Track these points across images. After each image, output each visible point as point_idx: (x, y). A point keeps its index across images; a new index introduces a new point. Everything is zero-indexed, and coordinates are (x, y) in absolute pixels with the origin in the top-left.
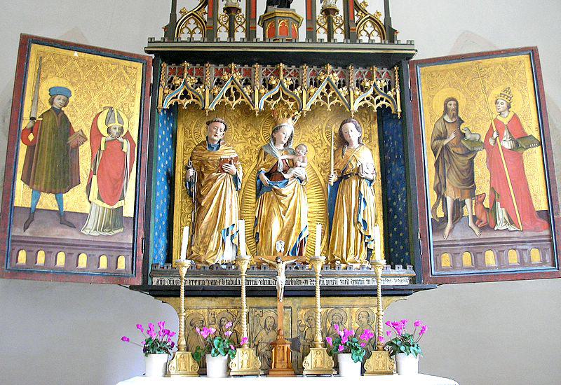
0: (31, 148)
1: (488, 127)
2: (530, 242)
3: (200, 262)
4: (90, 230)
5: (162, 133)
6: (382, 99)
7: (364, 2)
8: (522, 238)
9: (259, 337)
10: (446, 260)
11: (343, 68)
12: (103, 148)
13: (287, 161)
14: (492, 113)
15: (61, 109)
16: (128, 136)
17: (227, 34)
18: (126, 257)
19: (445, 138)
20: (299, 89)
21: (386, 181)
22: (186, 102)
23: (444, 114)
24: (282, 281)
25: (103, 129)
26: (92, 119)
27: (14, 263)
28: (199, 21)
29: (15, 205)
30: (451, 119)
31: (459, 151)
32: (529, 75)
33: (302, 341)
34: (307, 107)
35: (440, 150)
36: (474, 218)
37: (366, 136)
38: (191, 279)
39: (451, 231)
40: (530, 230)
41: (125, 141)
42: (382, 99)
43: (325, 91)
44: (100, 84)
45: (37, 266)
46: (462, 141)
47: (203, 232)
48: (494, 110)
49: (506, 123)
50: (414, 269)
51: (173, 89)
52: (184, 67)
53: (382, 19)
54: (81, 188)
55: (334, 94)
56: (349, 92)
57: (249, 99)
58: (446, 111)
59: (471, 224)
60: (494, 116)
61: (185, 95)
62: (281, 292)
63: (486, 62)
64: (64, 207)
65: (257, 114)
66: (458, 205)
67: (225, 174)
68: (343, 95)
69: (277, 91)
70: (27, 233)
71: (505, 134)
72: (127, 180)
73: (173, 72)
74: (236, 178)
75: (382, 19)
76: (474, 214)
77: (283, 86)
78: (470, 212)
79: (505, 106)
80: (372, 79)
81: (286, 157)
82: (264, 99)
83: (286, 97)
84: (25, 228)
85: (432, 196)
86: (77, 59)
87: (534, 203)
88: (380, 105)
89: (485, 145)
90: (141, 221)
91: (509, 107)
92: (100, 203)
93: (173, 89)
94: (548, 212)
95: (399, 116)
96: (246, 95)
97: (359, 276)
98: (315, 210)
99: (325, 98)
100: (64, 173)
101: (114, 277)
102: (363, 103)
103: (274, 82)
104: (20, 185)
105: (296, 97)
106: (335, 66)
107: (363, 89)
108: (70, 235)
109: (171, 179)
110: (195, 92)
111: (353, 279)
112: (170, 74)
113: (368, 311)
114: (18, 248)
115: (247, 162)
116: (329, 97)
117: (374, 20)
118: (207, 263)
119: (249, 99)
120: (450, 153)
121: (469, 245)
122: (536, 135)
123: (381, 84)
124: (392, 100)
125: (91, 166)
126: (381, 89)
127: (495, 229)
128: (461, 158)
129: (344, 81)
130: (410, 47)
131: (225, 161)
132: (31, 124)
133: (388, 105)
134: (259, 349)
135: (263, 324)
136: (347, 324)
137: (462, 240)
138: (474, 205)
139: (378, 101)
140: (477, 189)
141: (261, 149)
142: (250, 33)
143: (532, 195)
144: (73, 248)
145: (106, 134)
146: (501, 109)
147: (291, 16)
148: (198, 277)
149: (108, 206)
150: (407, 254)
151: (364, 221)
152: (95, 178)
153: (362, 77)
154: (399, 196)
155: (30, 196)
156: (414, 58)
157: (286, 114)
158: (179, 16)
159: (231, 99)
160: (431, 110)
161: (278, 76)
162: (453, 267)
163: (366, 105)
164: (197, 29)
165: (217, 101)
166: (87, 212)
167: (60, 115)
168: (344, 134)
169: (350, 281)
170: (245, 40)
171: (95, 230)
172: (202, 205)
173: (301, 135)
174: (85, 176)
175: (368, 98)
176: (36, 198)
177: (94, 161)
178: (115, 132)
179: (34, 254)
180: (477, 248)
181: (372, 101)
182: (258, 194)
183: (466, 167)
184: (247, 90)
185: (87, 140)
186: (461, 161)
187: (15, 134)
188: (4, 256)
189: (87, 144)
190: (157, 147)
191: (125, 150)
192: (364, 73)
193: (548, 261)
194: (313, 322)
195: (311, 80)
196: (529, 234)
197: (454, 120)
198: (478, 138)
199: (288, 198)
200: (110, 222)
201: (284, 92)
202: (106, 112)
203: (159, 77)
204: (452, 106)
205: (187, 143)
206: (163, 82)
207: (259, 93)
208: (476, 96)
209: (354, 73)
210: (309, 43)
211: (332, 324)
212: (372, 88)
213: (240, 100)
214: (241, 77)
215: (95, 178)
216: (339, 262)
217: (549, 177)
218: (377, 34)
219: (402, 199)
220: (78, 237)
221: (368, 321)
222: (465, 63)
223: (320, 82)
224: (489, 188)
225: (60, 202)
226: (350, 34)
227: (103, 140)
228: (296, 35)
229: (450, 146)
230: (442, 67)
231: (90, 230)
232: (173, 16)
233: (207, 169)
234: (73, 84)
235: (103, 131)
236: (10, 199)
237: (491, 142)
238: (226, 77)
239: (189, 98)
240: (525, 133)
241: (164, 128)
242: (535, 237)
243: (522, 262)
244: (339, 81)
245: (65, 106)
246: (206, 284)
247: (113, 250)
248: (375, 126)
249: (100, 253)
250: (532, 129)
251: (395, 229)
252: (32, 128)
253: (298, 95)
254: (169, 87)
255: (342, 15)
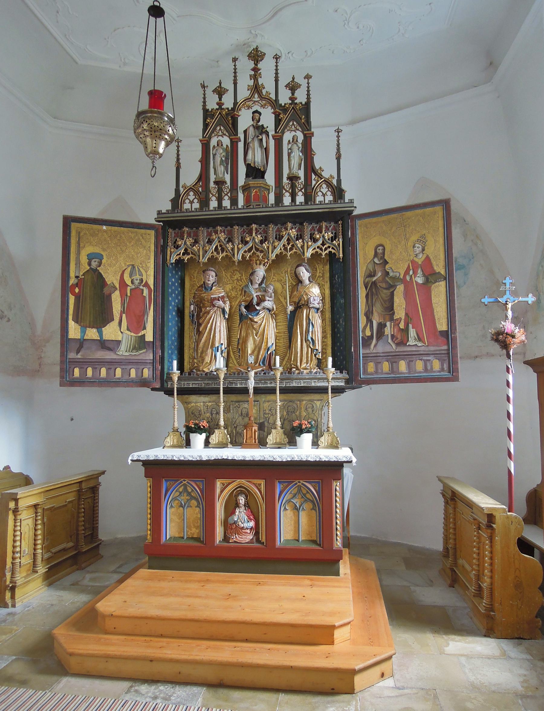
0: (78, 298)
1: (406, 266)
2: (433, 354)
3: (199, 371)
4: (123, 351)
5: (172, 280)
6: (329, 247)
7: (320, 168)
8: (428, 351)
9: (238, 421)
10: (371, 367)
11: (300, 225)
12: (129, 294)
13: (260, 296)
14: (410, 256)
15: (97, 268)
16: (147, 285)
17: (290, 198)
18: (149, 369)
19: (374, 276)
20: (266, 243)
21: (334, 308)
22: (186, 258)
23: (374, 258)
24: (251, 384)
25: (128, 281)
26: (120, 274)
27: (71, 376)
28: (196, 193)
29: (69, 337)
30: (379, 261)
31: (384, 285)
32: (441, 223)
33: (266, 424)
34: (273, 256)
35: (370, 285)
36: (393, 336)
37: (321, 275)
38: (193, 382)
39: (375, 346)
40: (434, 346)
41: (144, 288)
42: (329, 247)
43: (286, 244)
44: (124, 248)
45: (88, 378)
46: (387, 279)
47: (201, 350)
48: (411, 253)
49: (420, 263)
50: (348, 373)
51: (177, 248)
52: (184, 231)
53: (335, 182)
54: (114, 325)
55: (293, 246)
56: (304, 243)
57: (230, 253)
58: (376, 255)
59: (390, 341)
60: (411, 258)
61: (186, 253)
62: (251, 391)
63: (409, 214)
64: (104, 337)
65: (236, 264)
66: (382, 326)
67: (216, 308)
68: (299, 246)
69: (251, 245)
70: (79, 356)
71: (419, 272)
72: (147, 316)
73: (176, 235)
74: (224, 311)
75: (335, 182)
76: (392, 333)
77: (255, 241)
78: (389, 332)
79: (420, 249)
80: (321, 233)
81: (258, 294)
82: (241, 252)
83: (257, 250)
84: (78, 352)
85: (362, 320)
86: (105, 231)
87: (437, 325)
88: (327, 252)
89: (404, 281)
90: (158, 344)
91: (423, 250)
92: (129, 333)
93: (177, 248)
94: (447, 331)
95: (341, 260)
96: (228, 250)
97: (308, 379)
98: (282, 331)
99: (286, 249)
100: (102, 314)
101: (143, 383)
102: (315, 250)
103: (248, 239)
104: (72, 324)
105: (265, 249)
106: (294, 223)
107: (315, 241)
108: (108, 355)
109: (181, 313)
110: (192, 250)
111: (304, 381)
112: (175, 237)
113: (313, 403)
114: (74, 366)
115: (234, 298)
116: (289, 248)
117: (328, 183)
118: (204, 371)
119: (230, 253)
120: (377, 286)
121: (388, 356)
122: (443, 272)
123: (328, 235)
124: (337, 248)
125: (121, 308)
126: (329, 239)
127: (407, 344)
128: (385, 291)
129: (301, 235)
130: (351, 205)
131: (215, 299)
132: (76, 281)
133: (333, 251)
134: (238, 429)
135: (240, 413)
136: (298, 413)
137: (383, 353)
138: (392, 326)
139: (326, 249)
140: (396, 314)
141: (243, 288)
142: (234, 201)
143: (436, 319)
144: (111, 364)
145: (130, 285)
146: (417, 252)
147: (262, 185)
148: (197, 381)
149: (135, 335)
150: (344, 362)
151: (312, 339)
152: (124, 316)
153: (315, 230)
154: (341, 320)
155: (80, 331)
156: (355, 213)
157: (258, 262)
158: (181, 189)
159: (218, 253)
160: (365, 254)
161: (251, 234)
162: (376, 372)
163: (317, 252)
164: (196, 199)
165: (209, 255)
166: (120, 339)
167: (96, 273)
168: (298, 275)
169: (302, 382)
170: (217, 209)
171: (126, 351)
172: (200, 330)
173: (272, 276)
174: (117, 315)
175: (318, 247)
176: (84, 332)
177: (123, 304)
178: (137, 282)
179: (84, 370)
180: (393, 359)
181: (321, 249)
182: (241, 320)
183: (388, 298)
184: (230, 246)
185: (117, 289)
186: (385, 293)
187: (66, 289)
188: (64, 372)
189: (117, 293)
190: (168, 291)
191: (144, 295)
192: (316, 227)
193: (445, 369)
194: (274, 411)
195: (276, 235)
196: (432, 348)
197: (381, 261)
198: (398, 275)
199: (258, 324)
200: (137, 346)
201: (257, 246)
202: (129, 269)
203: (167, 240)
204: (381, 251)
205: (192, 286)
206: (170, 244)
207: (238, 248)
208: (399, 242)
209: (308, 228)
210: (292, 206)
211: (288, 412)
212: (321, 239)
213: (225, 254)
214: (225, 236)
215: (124, 316)
216: (295, 369)
217: (450, 305)
218: (330, 193)
219: (342, 322)
220: (115, 357)
221: (313, 411)
222: (392, 215)
223: (283, 237)
224: (404, 314)
225: (101, 334)
226: (309, 198)
227: (129, 288)
228: (266, 199)
229: (377, 282)
230: (374, 220)
231: (123, 351)
232: (177, 190)
233: (203, 304)
234: (104, 250)
235: (129, 282)
236: (66, 334)
237: (408, 278)
238: (214, 237)
239: (188, 254)
240: (434, 271)
241: (173, 276)
242: (437, 350)
243: (426, 370)
244: (297, 235)
245: (99, 266)
246: (203, 385)
247: (139, 364)
248: (328, 267)
249: (130, 367)
250: (440, 267)
251: (338, 344)
252: (77, 284)
253: (266, 247)
254: (174, 247)
255: (303, 181)
